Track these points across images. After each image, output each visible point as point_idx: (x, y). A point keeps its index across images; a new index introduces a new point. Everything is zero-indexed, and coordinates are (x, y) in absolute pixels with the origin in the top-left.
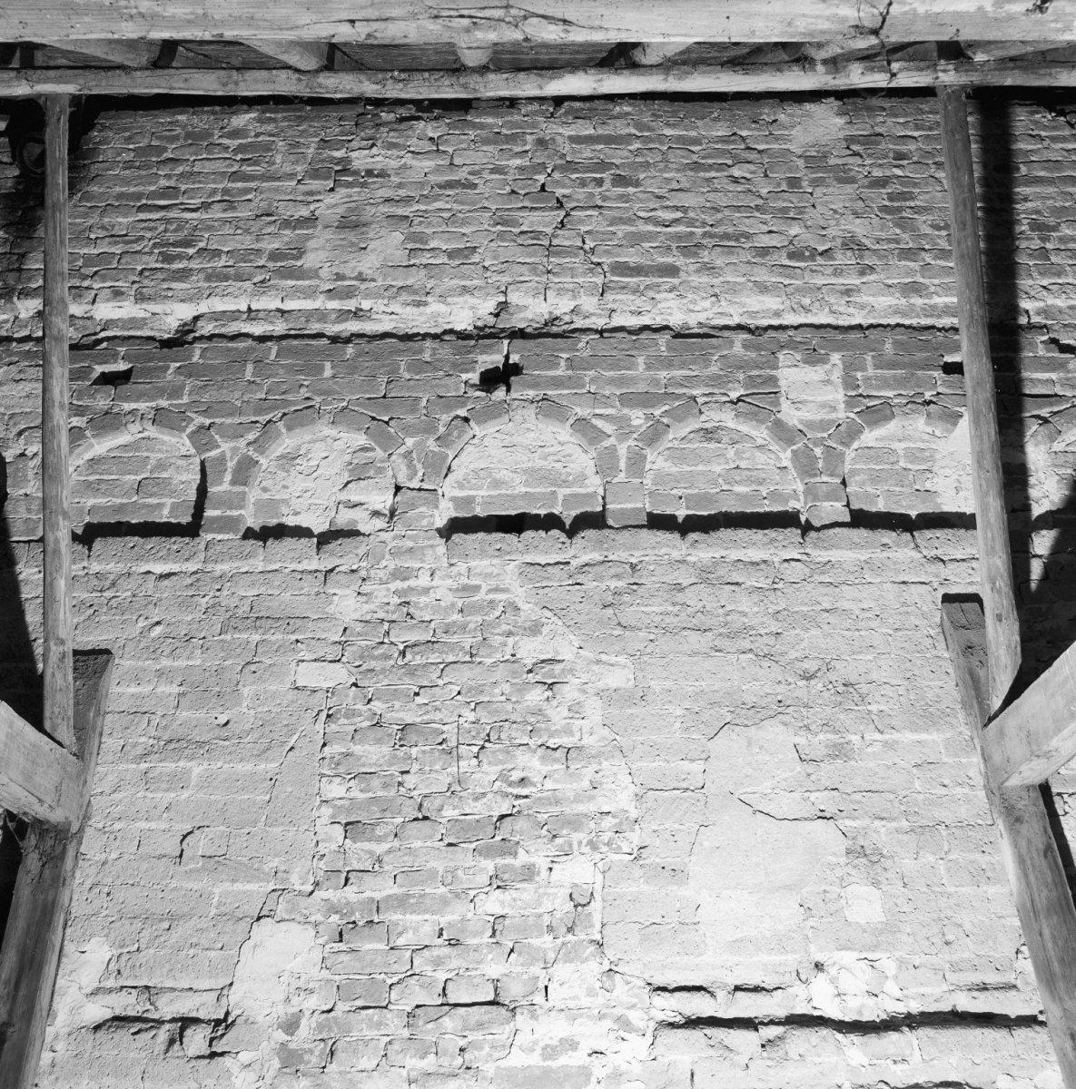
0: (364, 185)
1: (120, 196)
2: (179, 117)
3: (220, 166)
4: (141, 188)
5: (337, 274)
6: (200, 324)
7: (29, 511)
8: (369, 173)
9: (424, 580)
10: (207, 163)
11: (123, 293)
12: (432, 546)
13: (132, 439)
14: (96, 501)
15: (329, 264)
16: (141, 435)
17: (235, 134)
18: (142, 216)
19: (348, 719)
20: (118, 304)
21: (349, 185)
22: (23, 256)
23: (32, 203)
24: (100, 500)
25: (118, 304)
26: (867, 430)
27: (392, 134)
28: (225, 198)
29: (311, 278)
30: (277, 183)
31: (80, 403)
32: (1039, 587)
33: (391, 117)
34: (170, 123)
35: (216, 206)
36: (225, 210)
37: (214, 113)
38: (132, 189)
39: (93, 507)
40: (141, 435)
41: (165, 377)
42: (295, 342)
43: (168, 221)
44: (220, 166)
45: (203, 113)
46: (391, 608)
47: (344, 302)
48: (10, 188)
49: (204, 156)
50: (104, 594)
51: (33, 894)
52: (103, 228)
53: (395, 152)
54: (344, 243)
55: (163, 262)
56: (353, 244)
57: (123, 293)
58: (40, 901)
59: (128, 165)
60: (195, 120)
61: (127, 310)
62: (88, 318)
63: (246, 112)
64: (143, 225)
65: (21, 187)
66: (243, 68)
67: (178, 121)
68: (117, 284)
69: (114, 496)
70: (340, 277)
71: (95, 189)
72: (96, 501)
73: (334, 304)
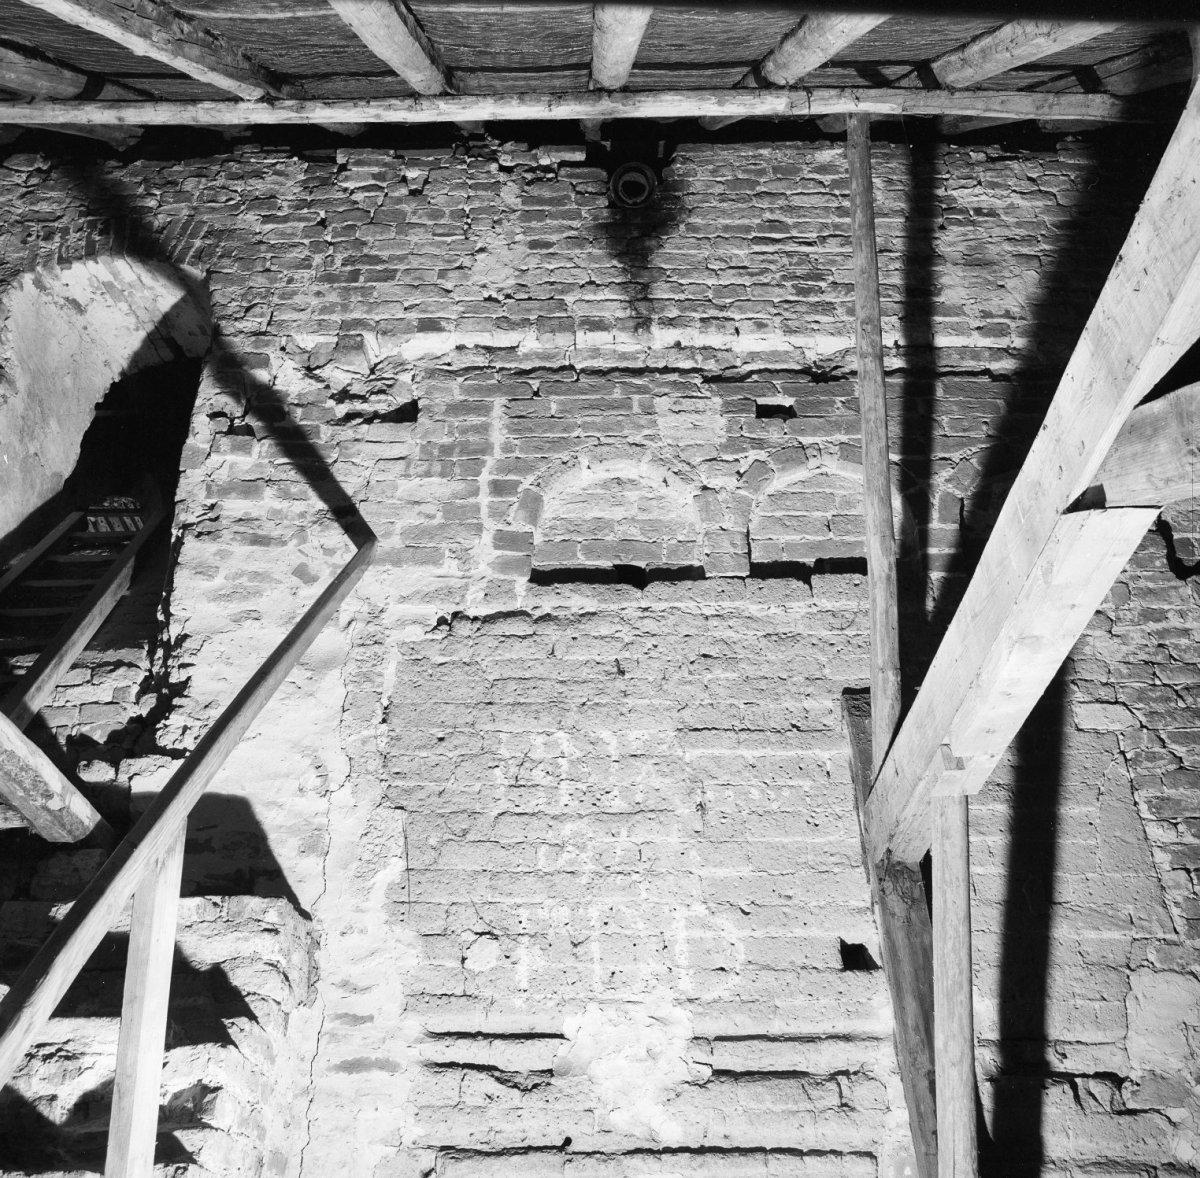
0: (973, 223)
1: (726, 228)
2: (762, 151)
3: (816, 201)
4: (746, 221)
5: (982, 311)
6: (848, 358)
7: (733, 545)
8: (978, 211)
9: (1175, 622)
10: (805, 198)
11: (766, 326)
12: (1175, 588)
13: (810, 475)
14: (788, 538)
15: (972, 301)
16: (818, 471)
17: (823, 169)
18: (757, 248)
19: (1152, 761)
20: (764, 336)
21: (959, 223)
22: (646, 287)
23: (636, 234)
24: (794, 537)
25: (764, 336)
26: (777, 475)
27: (989, 174)
28: (837, 233)
29: (958, 315)
30: (888, 220)
31: (752, 436)
32: (934, 617)
33: (981, 156)
34: (754, 157)
35: (830, 240)
36: (842, 245)
37: (798, 148)
38: (738, 222)
39: (787, 544)
40: (818, 471)
41: (833, 411)
42: (957, 379)
43: (789, 254)
44: (816, 201)
45: (787, 147)
46: (1152, 650)
47: (998, 340)
48: (607, 218)
49: (799, 191)
50: (845, 632)
51: (908, 936)
52: (721, 259)
53: (999, 192)
54: (980, 280)
55: (798, 294)
56: (989, 282)
57: (766, 326)
58: (918, 946)
59: (723, 198)
60: (779, 154)
61: (775, 341)
62: (727, 350)
63: (832, 147)
64: (762, 257)
65: (617, 217)
66: (194, 100)
67: (761, 155)
68: (756, 316)
69: (807, 533)
70: (986, 314)
71: (695, 220)
72: (788, 538)
73: (988, 342)
